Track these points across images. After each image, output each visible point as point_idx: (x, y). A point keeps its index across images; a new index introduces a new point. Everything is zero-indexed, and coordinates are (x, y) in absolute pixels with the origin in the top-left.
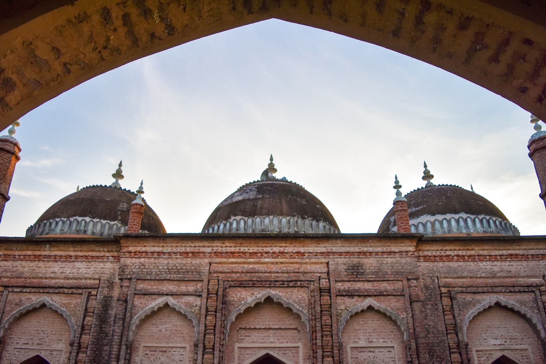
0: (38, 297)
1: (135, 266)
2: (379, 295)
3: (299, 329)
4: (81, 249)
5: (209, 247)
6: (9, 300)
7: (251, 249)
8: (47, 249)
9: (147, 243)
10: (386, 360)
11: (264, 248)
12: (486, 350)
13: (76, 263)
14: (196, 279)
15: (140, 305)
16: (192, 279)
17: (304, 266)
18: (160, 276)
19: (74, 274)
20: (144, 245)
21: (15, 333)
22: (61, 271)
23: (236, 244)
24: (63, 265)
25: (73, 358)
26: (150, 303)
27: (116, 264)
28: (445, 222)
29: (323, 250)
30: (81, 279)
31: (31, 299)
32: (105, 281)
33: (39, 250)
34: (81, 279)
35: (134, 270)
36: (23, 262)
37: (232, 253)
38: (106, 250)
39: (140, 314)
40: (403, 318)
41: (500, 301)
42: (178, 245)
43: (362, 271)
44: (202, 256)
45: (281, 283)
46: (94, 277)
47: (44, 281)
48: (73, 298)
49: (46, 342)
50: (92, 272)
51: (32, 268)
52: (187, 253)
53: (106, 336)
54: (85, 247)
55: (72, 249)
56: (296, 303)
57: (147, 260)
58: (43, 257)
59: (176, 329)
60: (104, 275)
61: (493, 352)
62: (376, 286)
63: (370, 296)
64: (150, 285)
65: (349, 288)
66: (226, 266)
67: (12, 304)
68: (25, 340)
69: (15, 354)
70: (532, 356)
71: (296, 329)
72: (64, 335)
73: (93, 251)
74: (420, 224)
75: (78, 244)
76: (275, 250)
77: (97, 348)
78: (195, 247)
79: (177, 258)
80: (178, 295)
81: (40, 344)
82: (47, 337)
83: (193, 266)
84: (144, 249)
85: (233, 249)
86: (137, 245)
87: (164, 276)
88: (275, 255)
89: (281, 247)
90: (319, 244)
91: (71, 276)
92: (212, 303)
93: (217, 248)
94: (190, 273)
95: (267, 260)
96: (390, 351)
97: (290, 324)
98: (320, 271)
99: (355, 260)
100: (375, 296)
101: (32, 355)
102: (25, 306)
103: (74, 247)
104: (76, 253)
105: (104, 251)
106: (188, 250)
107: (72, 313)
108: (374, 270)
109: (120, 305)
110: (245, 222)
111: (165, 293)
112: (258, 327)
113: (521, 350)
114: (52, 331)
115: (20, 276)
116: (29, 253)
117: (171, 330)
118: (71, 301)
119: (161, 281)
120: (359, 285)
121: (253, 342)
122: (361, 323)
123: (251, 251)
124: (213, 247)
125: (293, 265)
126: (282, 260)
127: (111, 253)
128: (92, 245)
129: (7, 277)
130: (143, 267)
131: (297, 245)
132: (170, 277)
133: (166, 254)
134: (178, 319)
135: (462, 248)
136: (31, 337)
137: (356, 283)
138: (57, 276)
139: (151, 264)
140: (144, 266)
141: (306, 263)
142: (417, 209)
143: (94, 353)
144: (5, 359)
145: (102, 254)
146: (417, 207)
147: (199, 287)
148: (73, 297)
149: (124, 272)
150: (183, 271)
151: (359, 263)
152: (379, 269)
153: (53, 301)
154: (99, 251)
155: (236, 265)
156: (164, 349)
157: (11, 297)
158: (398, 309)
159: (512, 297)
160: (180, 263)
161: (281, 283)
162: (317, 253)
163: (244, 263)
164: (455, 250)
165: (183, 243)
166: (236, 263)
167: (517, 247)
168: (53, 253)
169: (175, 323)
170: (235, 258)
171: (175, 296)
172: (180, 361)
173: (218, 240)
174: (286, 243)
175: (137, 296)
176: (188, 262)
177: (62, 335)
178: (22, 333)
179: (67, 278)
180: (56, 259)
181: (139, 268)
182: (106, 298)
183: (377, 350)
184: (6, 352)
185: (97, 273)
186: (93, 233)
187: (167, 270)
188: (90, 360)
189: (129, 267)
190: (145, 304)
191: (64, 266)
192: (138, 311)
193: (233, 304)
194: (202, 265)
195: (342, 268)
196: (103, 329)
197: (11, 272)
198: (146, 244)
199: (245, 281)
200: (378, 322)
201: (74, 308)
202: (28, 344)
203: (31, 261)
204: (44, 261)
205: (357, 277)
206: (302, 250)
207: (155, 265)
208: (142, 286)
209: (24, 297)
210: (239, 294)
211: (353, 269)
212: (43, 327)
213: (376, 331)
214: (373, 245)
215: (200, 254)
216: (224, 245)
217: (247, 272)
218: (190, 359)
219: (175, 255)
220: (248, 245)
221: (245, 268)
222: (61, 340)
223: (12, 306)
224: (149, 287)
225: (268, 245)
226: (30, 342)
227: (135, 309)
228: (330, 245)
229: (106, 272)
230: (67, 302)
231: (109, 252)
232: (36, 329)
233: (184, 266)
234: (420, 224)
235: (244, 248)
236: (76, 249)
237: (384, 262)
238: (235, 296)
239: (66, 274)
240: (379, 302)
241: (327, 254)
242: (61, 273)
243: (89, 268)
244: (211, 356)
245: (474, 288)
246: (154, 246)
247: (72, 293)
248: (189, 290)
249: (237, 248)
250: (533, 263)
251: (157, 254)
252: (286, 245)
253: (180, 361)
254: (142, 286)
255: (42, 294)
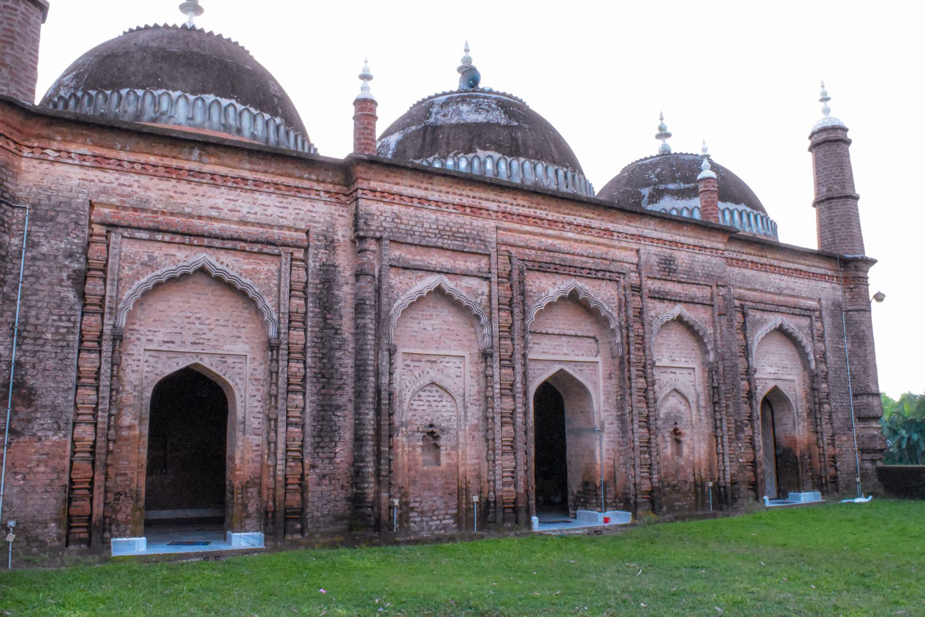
0: (188, 253)
1: (386, 217)
2: (690, 301)
3: (598, 338)
4: (266, 169)
5: (493, 201)
6: (125, 255)
7: (550, 214)
8: (193, 158)
9: (402, 178)
10: (687, 384)
11: (566, 216)
12: (763, 379)
13: (257, 195)
14: (480, 251)
15: (399, 285)
16: (475, 251)
17: (612, 250)
18: (427, 239)
19: (259, 216)
20: (395, 182)
21: (140, 320)
22: (231, 205)
23: (532, 203)
24: (233, 194)
25: (283, 369)
26: (414, 284)
27: (333, 207)
28: (727, 213)
29: (633, 230)
30: (272, 227)
31: (174, 255)
32: (318, 236)
33: (174, 158)
34: (272, 227)
35: (384, 224)
36: (143, 177)
37: (526, 217)
38: (314, 177)
39: (403, 300)
40: (710, 334)
41: (443, 286)
42: (450, 190)
43: (675, 268)
44: (484, 216)
45: (588, 271)
46: (298, 226)
47: (197, 222)
48: (261, 262)
49: (209, 339)
50: (293, 217)
51: (166, 193)
52: (463, 206)
53: (336, 333)
54: (274, 165)
55: (248, 166)
56: (605, 302)
57: (403, 209)
58: (187, 173)
59: (448, 327)
60: (315, 225)
61: (767, 381)
62: (686, 290)
63: (680, 301)
64: (409, 253)
65: (659, 288)
66: (517, 235)
67: (133, 263)
68: (165, 334)
69: (147, 361)
70: (798, 389)
71: (594, 338)
72: (244, 327)
73: (289, 176)
74: (696, 209)
75: (262, 159)
76: (579, 222)
77: (323, 354)
78: (474, 197)
79: (450, 213)
80: (456, 274)
81: (199, 343)
82: (211, 330)
83: (474, 229)
84: (396, 189)
85: (526, 211)
86: (385, 179)
87: (433, 241)
88: (579, 229)
89: (587, 218)
90: (630, 221)
91: (251, 218)
92: (504, 291)
93: (505, 205)
94: (471, 241)
95: (570, 235)
96: (690, 374)
97: (588, 331)
98: (630, 261)
99: (667, 252)
100: (685, 302)
101: (183, 363)
102: (164, 270)
103: (251, 163)
104: (260, 176)
105: (309, 179)
106: (465, 201)
107: (265, 289)
108: (685, 269)
109: (370, 282)
110: (510, 166)
111: (438, 269)
112: (550, 331)
113: (790, 381)
114: (218, 320)
115: (141, 206)
116: (152, 159)
117: (440, 329)
118: (258, 268)
119: (426, 249)
120: (670, 287)
121: (544, 353)
122: (665, 335)
123: (550, 218)
124: (500, 202)
125: (599, 247)
126: (588, 238)
127: (323, 185)
128: (288, 165)
129: (111, 206)
130: (399, 221)
131: (606, 219)
132: (443, 243)
133: (431, 203)
134: (449, 312)
135: (758, 253)
136: (178, 330)
137: (667, 282)
138: (222, 215)
139: (411, 217)
140: (401, 219)
141: (614, 247)
142: (687, 186)
143: (320, 362)
144: (128, 370)
145: (306, 184)
146: (688, 183)
147: (483, 266)
148: (261, 260)
149: (369, 225)
150: (461, 235)
151: (671, 257)
152: (690, 268)
153: (222, 263)
154: (301, 178)
155: (531, 237)
156: (433, 359)
157: (129, 248)
158: (706, 322)
159: (793, 320)
160: (455, 221)
161: (588, 271)
162: (627, 234)
163: (542, 235)
164: (750, 254)
165: (458, 189)
166: (531, 233)
167: (803, 262)
168: (207, 168)
169: (445, 319)
170: (530, 225)
171: (451, 276)
172: (457, 376)
173: (508, 192)
174: (593, 213)
175: (393, 270)
176: (468, 223)
177: (238, 327)
178: (155, 320)
179: (243, 222)
180: (215, 180)
181: (393, 221)
182: (325, 268)
183: (678, 371)
184: (127, 357)
185: (302, 220)
186: (254, 136)
187: (437, 231)
188: (315, 373)
189: (376, 218)
190: (407, 284)
191: (236, 198)
192: (398, 296)
193: (531, 297)
194: (487, 229)
195: (654, 260)
196: (329, 321)
197: (118, 195)
198: (398, 180)
199: (546, 263)
200: (680, 336)
201: (266, 281)
202: (173, 342)
203: (161, 177)
204: (189, 182)
205: (669, 275)
206: (611, 226)
207: (417, 220)
208: (397, 253)
209: (159, 251)
210: (538, 282)
211: (665, 264)
212: (197, 311)
213: (678, 347)
214: (686, 234)
215: (482, 211)
216: (515, 203)
217: (545, 250)
218: (472, 374)
219: (446, 206)
220: (547, 207)
221: (543, 242)
222: (239, 337)
223: (135, 266)
224: (409, 256)
225: (572, 212)
226: (177, 339)
227: (393, 292)
228: (641, 226)
229: (317, 219)
230: (250, 267)
231: (318, 181)
232: (183, 314)
233: (461, 228)
234: (696, 209)
235: (541, 211)
236: (256, 167)
237: (696, 259)
238: (532, 284)
239: (241, 214)
240: (688, 310)
241: (639, 237)
242: (231, 211)
243: (284, 208)
244: (510, 371)
245: (763, 305)
246: (411, 186)
247: (260, 253)
248: (470, 268)
249: (532, 210)
250: (813, 283)
251: (417, 201)
252: (593, 216)
253: (457, 376)
254: (397, 253)
255: (197, 249)
